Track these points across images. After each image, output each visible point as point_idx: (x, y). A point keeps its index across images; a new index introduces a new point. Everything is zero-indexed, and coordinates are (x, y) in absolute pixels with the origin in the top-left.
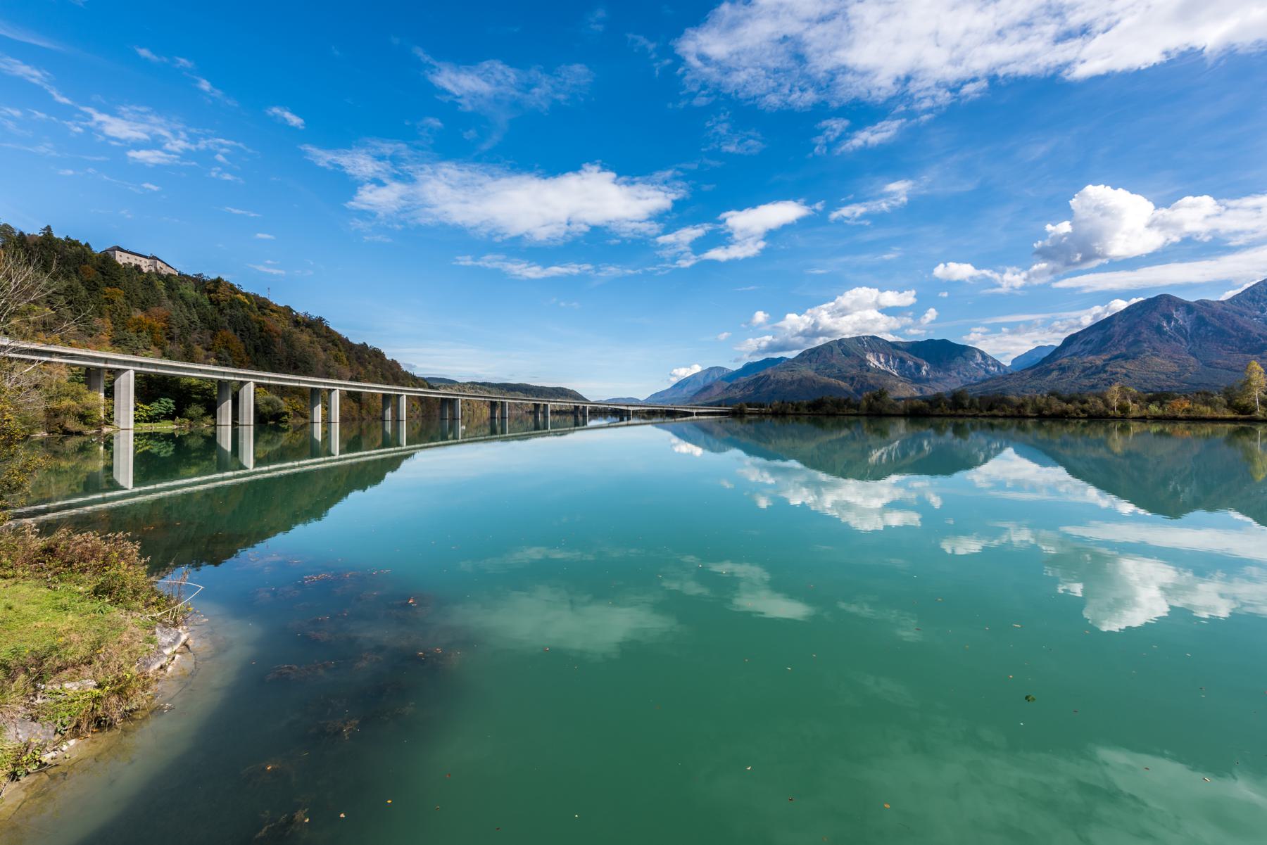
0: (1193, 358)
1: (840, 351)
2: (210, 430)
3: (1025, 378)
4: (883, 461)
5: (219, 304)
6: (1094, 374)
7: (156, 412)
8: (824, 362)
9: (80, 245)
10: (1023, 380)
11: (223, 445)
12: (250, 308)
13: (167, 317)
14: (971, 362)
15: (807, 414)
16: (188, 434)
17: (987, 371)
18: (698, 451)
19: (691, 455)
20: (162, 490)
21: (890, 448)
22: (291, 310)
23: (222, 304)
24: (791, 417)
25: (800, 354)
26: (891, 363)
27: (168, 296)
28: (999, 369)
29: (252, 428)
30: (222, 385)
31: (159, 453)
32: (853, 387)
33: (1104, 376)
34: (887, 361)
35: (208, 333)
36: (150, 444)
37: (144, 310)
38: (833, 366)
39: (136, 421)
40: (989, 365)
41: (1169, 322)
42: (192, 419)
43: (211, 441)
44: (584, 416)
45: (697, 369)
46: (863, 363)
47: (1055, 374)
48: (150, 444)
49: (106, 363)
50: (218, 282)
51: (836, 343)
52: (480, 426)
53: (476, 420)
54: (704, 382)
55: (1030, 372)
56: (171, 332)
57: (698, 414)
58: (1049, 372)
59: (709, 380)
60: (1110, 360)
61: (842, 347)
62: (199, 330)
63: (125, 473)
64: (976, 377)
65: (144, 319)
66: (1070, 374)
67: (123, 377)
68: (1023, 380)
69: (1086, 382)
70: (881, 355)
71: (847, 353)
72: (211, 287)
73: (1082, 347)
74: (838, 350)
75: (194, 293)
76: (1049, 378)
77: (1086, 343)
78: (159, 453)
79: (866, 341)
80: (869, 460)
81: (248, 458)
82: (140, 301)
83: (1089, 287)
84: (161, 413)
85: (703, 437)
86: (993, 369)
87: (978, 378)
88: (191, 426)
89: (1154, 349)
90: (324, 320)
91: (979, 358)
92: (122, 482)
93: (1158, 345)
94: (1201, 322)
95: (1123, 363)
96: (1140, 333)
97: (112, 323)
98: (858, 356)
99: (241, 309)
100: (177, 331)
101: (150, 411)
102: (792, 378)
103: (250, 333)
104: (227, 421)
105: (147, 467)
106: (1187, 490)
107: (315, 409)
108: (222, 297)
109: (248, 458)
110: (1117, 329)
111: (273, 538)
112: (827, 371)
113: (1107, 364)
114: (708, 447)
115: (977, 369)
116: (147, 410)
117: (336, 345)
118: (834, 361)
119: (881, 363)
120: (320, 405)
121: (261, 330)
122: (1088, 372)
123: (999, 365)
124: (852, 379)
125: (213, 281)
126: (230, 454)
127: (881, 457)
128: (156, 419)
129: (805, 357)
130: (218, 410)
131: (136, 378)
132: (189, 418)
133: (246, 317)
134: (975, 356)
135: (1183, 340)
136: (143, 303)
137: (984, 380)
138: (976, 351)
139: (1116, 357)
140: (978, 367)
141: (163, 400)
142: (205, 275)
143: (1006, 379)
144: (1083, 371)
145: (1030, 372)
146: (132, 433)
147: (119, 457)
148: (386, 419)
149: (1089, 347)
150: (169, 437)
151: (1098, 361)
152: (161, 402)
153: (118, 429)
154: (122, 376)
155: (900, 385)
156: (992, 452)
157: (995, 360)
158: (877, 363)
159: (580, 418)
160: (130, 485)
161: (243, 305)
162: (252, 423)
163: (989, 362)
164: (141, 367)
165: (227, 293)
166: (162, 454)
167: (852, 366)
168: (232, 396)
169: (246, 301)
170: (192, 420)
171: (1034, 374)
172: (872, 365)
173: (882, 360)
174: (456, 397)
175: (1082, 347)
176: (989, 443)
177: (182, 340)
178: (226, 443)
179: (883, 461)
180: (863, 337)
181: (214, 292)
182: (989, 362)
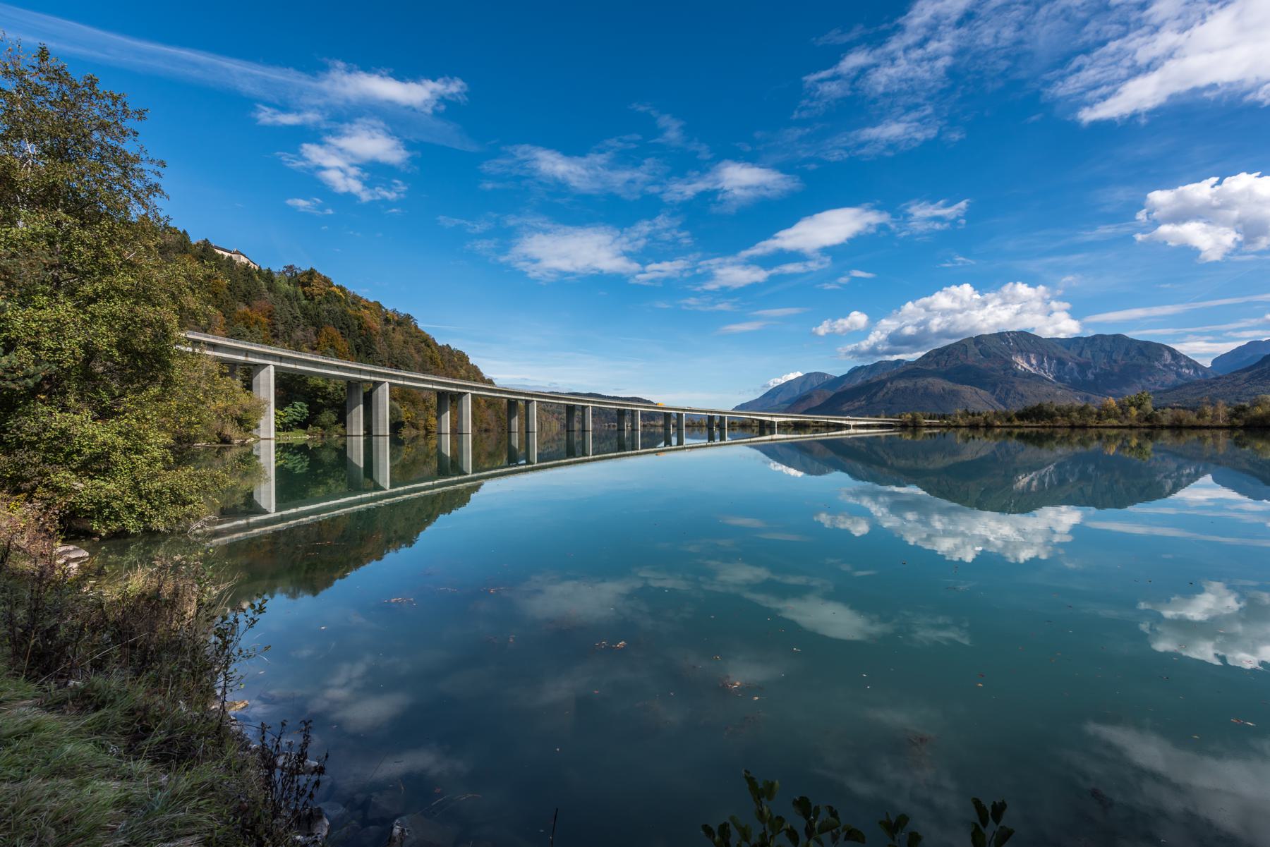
1: (977, 351)
2: (340, 442)
3: (1237, 382)
4: (1033, 489)
5: (313, 299)
7: (291, 418)
9: (179, 233)
10: (1237, 386)
11: (355, 461)
12: (346, 302)
13: (270, 311)
14: (1156, 364)
15: (1096, 427)
16: (322, 447)
17: (1179, 375)
18: (800, 474)
19: (795, 477)
20: (308, 512)
21: (1043, 472)
22: (380, 306)
23: (317, 299)
24: (1166, 423)
25: (923, 356)
26: (1046, 365)
27: (268, 289)
28: (1196, 371)
29: (388, 438)
30: (352, 385)
31: (294, 468)
34: (1041, 363)
35: (312, 329)
36: (285, 458)
37: (247, 304)
39: (278, 430)
40: (1182, 367)
42: (324, 427)
43: (342, 452)
44: (679, 430)
45: (799, 374)
46: (1008, 365)
48: (285, 458)
49: (247, 356)
50: (311, 273)
51: (972, 342)
52: (549, 442)
53: (544, 435)
54: (800, 390)
55: (1246, 375)
56: (275, 328)
57: (856, 427)
59: (807, 388)
61: (980, 346)
62: (302, 326)
63: (267, 495)
64: (1163, 383)
65: (250, 314)
67: (262, 374)
68: (1237, 386)
70: (1032, 356)
71: (986, 354)
72: (305, 279)
74: (974, 350)
75: (288, 287)
78: (294, 468)
79: (1013, 339)
80: (1014, 487)
81: (384, 474)
82: (241, 293)
84: (295, 420)
85: (798, 456)
86: (1187, 371)
87: (1166, 383)
88: (322, 435)
90: (412, 318)
91: (1168, 358)
92: (264, 505)
97: (224, 316)
98: (1001, 357)
99: (337, 304)
100: (281, 328)
101: (284, 417)
102: (915, 385)
103: (349, 331)
104: (359, 430)
105: (290, 488)
107: (443, 416)
108: (316, 291)
109: (384, 474)
111: (367, 565)
114: (809, 471)
115: (1164, 371)
116: (281, 416)
117: (429, 346)
119: (1031, 365)
120: (449, 412)
121: (360, 327)
123: (1195, 366)
125: (306, 273)
126: (362, 471)
127: (1030, 483)
128: (289, 427)
129: (931, 359)
130: (348, 416)
131: (276, 372)
132: (321, 427)
133: (344, 312)
134: (1162, 355)
136: (245, 296)
137: (1176, 387)
140: (1166, 369)
141: (297, 404)
142: (297, 266)
143: (1211, 384)
145: (1246, 375)
146: (273, 443)
150: (303, 448)
152: (296, 406)
153: (258, 439)
154: (261, 373)
155: (1059, 392)
156: (1184, 479)
157: (1191, 360)
158: (1026, 365)
159: (717, 433)
160: (273, 509)
161: (339, 299)
162: (388, 433)
164: (281, 362)
165: (322, 286)
166: (298, 471)
168: (364, 398)
169: (341, 294)
170: (324, 429)
171: (1252, 377)
172: (1020, 368)
173: (1034, 362)
174: (586, 404)
176: (1179, 468)
177: (287, 337)
178: (358, 458)
179: (1033, 489)
180: (1008, 333)
181: (308, 285)
182: (1183, 363)
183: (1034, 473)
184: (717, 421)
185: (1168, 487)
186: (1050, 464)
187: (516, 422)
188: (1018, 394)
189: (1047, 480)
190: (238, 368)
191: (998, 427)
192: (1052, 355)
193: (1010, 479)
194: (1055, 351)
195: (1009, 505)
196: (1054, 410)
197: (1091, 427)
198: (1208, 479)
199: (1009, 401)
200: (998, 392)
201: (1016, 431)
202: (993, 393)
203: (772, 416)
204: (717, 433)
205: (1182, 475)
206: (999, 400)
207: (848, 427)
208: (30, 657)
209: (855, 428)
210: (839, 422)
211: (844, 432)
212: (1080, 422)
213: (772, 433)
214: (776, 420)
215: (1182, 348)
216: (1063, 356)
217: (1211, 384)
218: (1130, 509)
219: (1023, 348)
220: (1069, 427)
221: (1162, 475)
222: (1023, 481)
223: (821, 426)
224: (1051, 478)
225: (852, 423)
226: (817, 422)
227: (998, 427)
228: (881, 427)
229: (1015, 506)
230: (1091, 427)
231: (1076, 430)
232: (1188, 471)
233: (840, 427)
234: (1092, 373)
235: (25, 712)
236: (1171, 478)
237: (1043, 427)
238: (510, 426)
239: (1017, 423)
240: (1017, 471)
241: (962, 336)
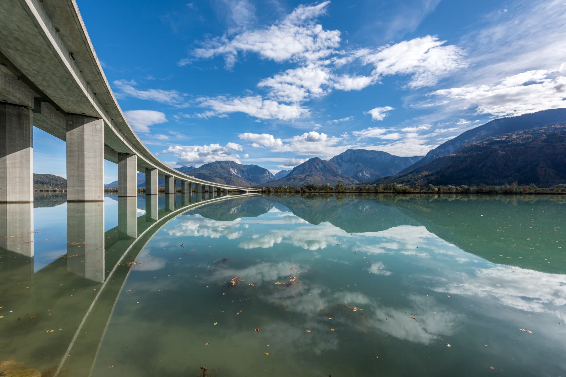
0: (323, 177)
1: (220, 166)
6: (302, 180)
8: (213, 170)
15: (308, 192)
17: (270, 178)
28: (273, 177)
32: (226, 182)
33: (305, 181)
38: (217, 172)
41: (318, 166)
46: (229, 172)
47: (292, 180)
55: (285, 179)
58: (291, 179)
60: (306, 176)
61: (220, 165)
66: (296, 180)
69: (301, 183)
70: (235, 169)
71: (222, 167)
73: (298, 171)
74: (218, 166)
76: (291, 181)
77: (299, 170)
83: (382, 146)
89: (315, 174)
91: (267, 172)
93: (316, 172)
94: (325, 166)
95: (309, 177)
96: (312, 168)
106: (320, 216)
110: (306, 166)
112: (215, 174)
113: (306, 178)
118: (217, 170)
119: (235, 172)
122: (301, 180)
124: (226, 178)
127: (234, 211)
134: (266, 172)
135: (321, 171)
138: (267, 172)
139: (307, 176)
144: (300, 179)
147: (32, 142)
148: (170, 192)
149: (300, 172)
151: (303, 176)
156: (270, 207)
158: (234, 172)
163: (270, 175)
167: (224, 173)
173: (236, 171)
175: (298, 171)
176: (270, 204)
180: (229, 161)
183: (236, 207)
185: (267, 209)
188: (233, 181)
190: (339, 158)
195: (228, 218)
200: (227, 180)
202: (225, 181)
203: (226, 186)
205: (270, 206)
210: (244, 190)
213: (225, 195)
214: (227, 188)
215: (270, 171)
217: (278, 181)
220: (295, 192)
221: (266, 206)
229: (230, 218)
232: (271, 205)
240: (231, 207)
241: (297, 165)
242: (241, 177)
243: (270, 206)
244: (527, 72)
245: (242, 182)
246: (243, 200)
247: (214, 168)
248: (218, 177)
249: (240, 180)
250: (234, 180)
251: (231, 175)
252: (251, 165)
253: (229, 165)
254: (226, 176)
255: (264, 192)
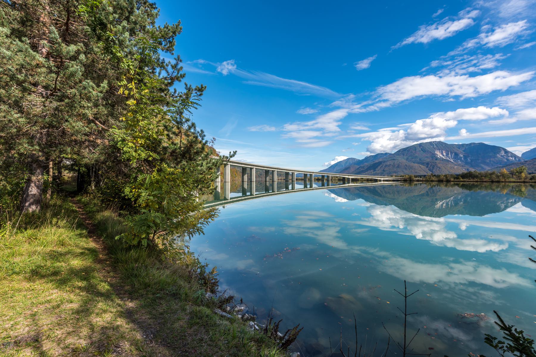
1: (420, 149)
4: (444, 207)
14: (498, 155)
17: (508, 160)
18: (344, 200)
21: (448, 200)
26: (450, 155)
34: (447, 155)
38: (416, 157)
40: (509, 157)
46: (434, 156)
57: (384, 181)
70: (444, 151)
74: (419, 149)
79: (435, 144)
86: (511, 158)
118: (417, 155)
119: (443, 155)
124: (428, 164)
127: (442, 205)
157: (513, 154)
158: (441, 156)
167: (427, 157)
179: (444, 207)
182: (509, 155)
183: (444, 201)
184: (308, 176)
186: (451, 197)
187: (246, 177)
189: (450, 203)
191: (453, 181)
192: (452, 151)
193: (434, 202)
194: (454, 149)
196: (477, 174)
197: (502, 182)
198: (519, 204)
199: (434, 170)
200: (429, 166)
201: (462, 183)
202: (427, 167)
204: (308, 183)
205: (509, 202)
206: (430, 170)
207: (380, 181)
208: (20, 222)
209: (383, 181)
211: (379, 183)
212: (497, 180)
213: (349, 183)
214: (350, 177)
216: (457, 152)
217: (523, 164)
218: (486, 216)
219: (440, 148)
220: (491, 182)
222: (439, 204)
223: (365, 180)
224: (451, 202)
225: (382, 179)
226: (362, 178)
227: (453, 181)
228: (393, 181)
230: (502, 182)
231: (494, 183)
232: (511, 201)
233: (376, 181)
234: (470, 159)
235: (21, 355)
236: (504, 203)
237: (477, 182)
238: (243, 179)
239: (462, 180)
240: (437, 200)
242: (452, 161)
243: (509, 202)
244: (476, 77)
245: (454, 168)
246: (455, 192)
247: (413, 152)
248: (418, 163)
249: (450, 165)
250: (439, 165)
251: (437, 159)
252: (471, 144)
253: (434, 147)
254: (428, 160)
255: (405, 181)
